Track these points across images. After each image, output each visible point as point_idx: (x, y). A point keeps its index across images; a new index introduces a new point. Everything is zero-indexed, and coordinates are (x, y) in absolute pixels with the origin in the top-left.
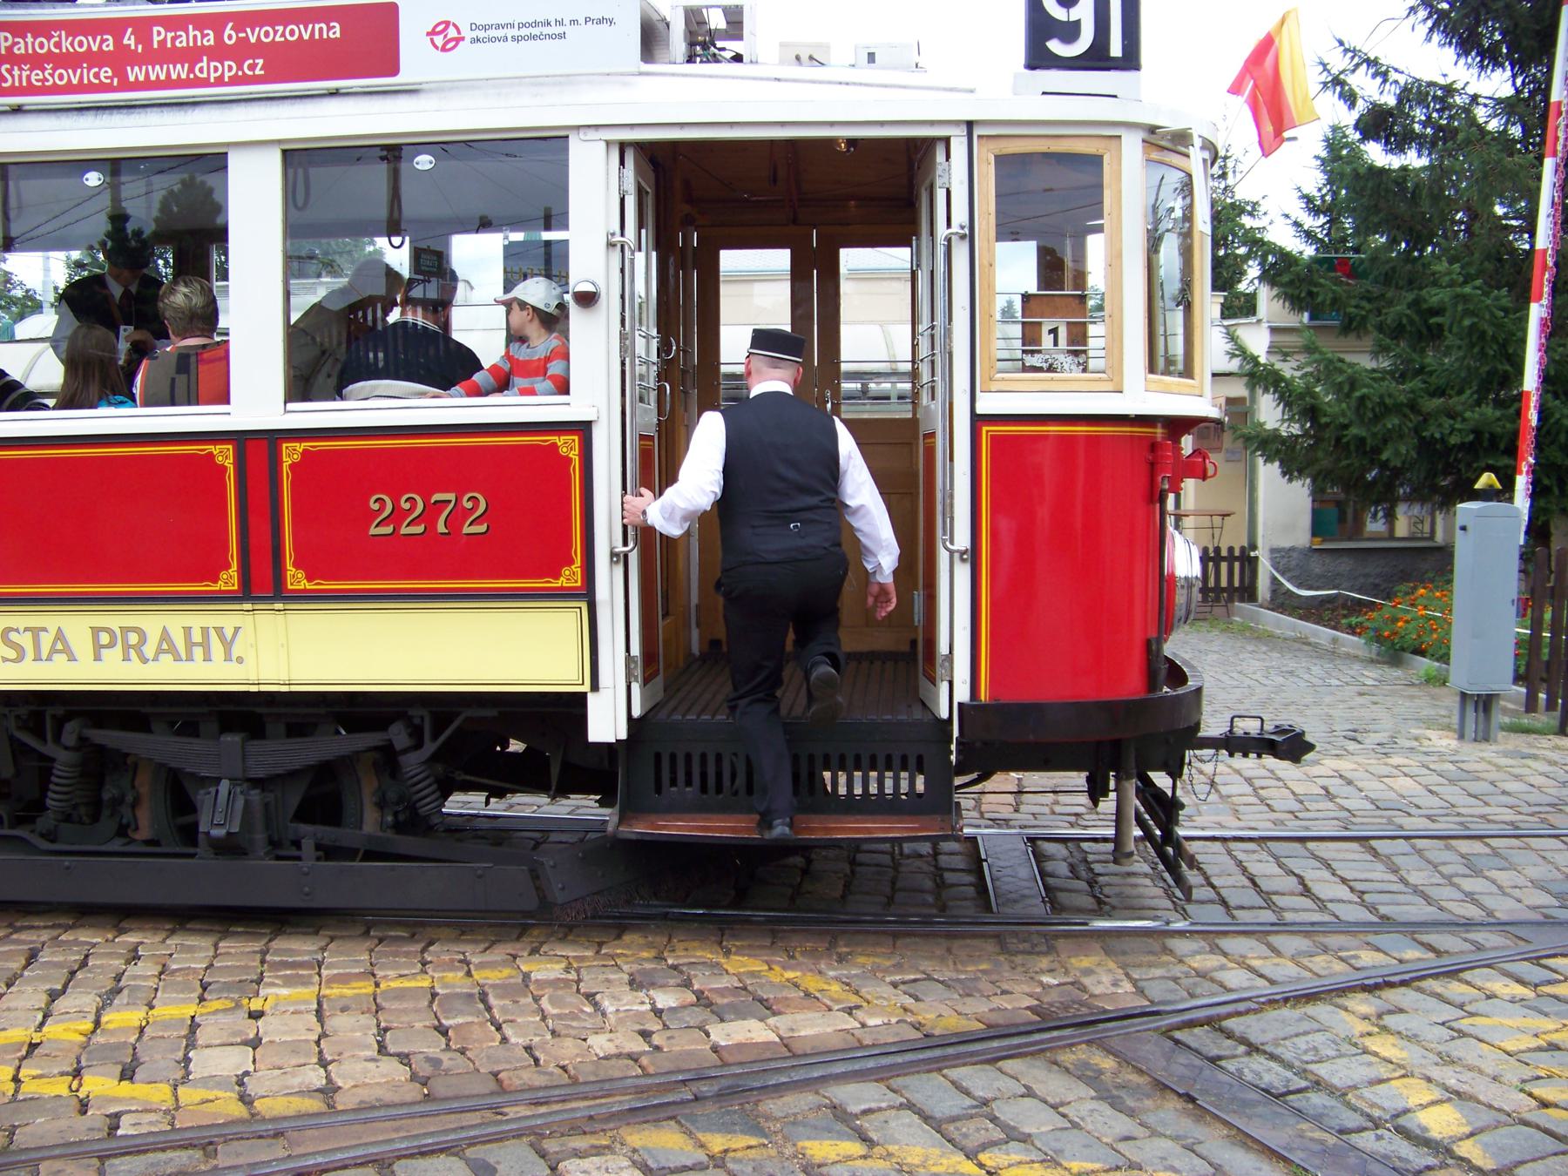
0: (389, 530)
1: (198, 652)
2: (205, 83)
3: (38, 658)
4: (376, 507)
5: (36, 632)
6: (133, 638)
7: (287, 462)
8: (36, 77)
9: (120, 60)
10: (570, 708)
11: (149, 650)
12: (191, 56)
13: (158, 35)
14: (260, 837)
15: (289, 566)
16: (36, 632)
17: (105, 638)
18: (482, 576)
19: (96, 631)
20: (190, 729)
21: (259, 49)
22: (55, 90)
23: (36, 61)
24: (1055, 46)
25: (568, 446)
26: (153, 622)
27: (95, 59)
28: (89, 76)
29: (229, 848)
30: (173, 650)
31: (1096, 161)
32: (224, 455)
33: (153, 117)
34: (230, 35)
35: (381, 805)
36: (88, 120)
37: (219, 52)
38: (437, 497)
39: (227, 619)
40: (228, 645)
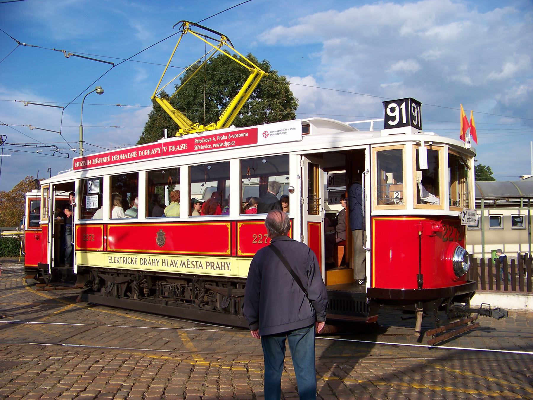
0: (256, 242)
4: (254, 237)
7: (109, 228)
12: (223, 141)
14: (232, 310)
15: (239, 250)
23: (199, 144)
24: (391, 123)
27: (209, 143)
32: (228, 225)
37: (228, 140)
38: (265, 235)
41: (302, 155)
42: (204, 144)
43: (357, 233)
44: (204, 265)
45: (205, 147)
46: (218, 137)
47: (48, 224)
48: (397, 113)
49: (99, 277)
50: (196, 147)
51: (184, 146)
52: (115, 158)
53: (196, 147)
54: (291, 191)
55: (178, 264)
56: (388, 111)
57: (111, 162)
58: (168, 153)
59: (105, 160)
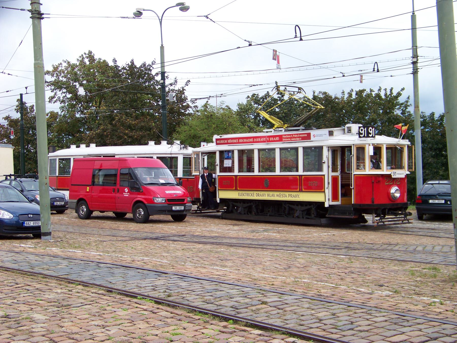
0: (387, 184)
7: (238, 178)
12: (296, 138)
14: (301, 217)
20: (297, 205)
23: (285, 138)
24: (361, 136)
25: (323, 177)
27: (289, 138)
29: (298, 217)
31: (381, 147)
33: (293, 144)
37: (298, 137)
41: (328, 147)
42: (287, 138)
43: (290, 179)
44: (288, 196)
45: (287, 140)
46: (294, 135)
47: (199, 175)
48: (363, 132)
49: (232, 204)
50: (284, 140)
51: (277, 138)
52: (241, 141)
53: (284, 140)
54: (324, 163)
55: (275, 196)
56: (360, 130)
57: (239, 143)
58: (269, 141)
59: (235, 141)
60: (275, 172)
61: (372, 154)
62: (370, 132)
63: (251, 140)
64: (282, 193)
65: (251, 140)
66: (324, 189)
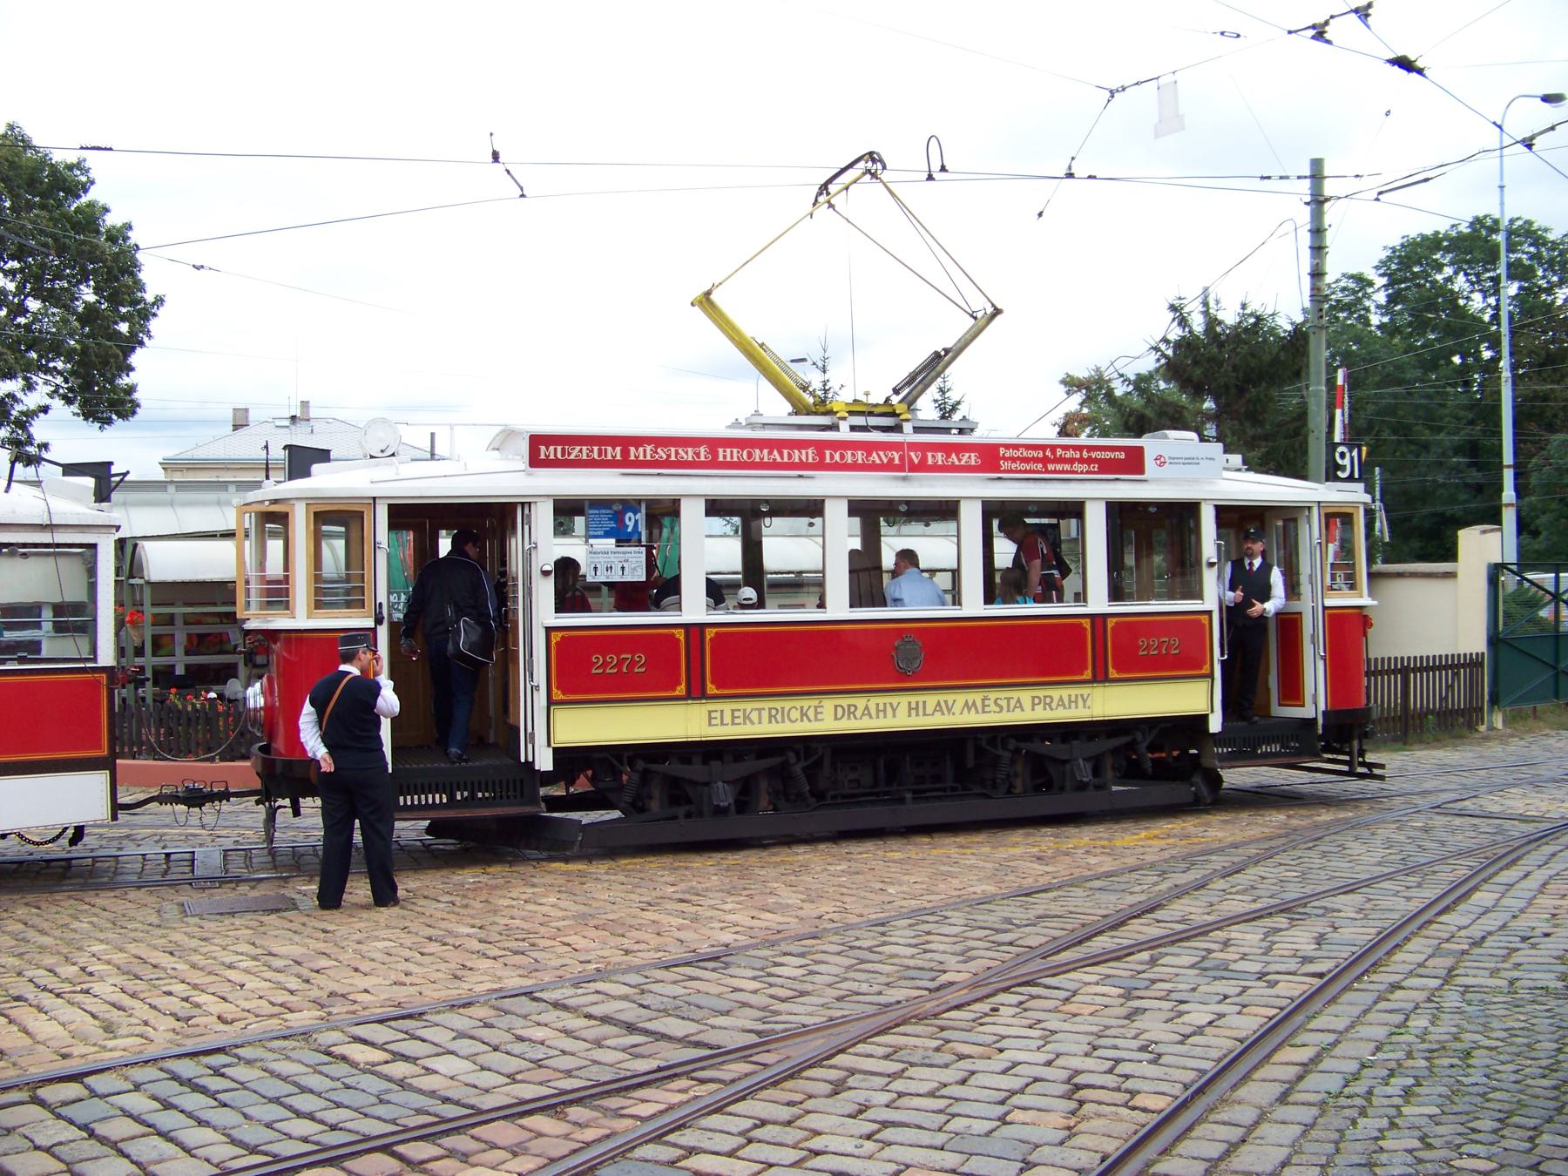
1: (1073, 705)
2: (1076, 472)
3: (925, 715)
5: (1008, 699)
6: (1048, 700)
8: (1014, 465)
9: (1045, 461)
10: (1202, 720)
11: (858, 714)
12: (1071, 461)
13: (1059, 452)
16: (1008, 699)
17: (1037, 701)
18: (813, 685)
19: (1033, 698)
21: (1095, 461)
22: (1020, 472)
23: (1013, 460)
25: (1204, 618)
26: (1056, 693)
27: (1036, 460)
28: (1033, 466)
30: (1063, 705)
32: (1086, 623)
34: (1085, 454)
35: (1114, 769)
36: (1031, 484)
37: (1081, 461)
39: (1084, 691)
40: (1084, 701)
42: (1025, 460)
48: (1346, 462)
50: (1004, 465)
53: (1004, 465)
60: (678, 606)
61: (613, 541)
62: (1340, 461)
63: (810, 455)
64: (993, 695)
65: (810, 455)
66: (1208, 666)
